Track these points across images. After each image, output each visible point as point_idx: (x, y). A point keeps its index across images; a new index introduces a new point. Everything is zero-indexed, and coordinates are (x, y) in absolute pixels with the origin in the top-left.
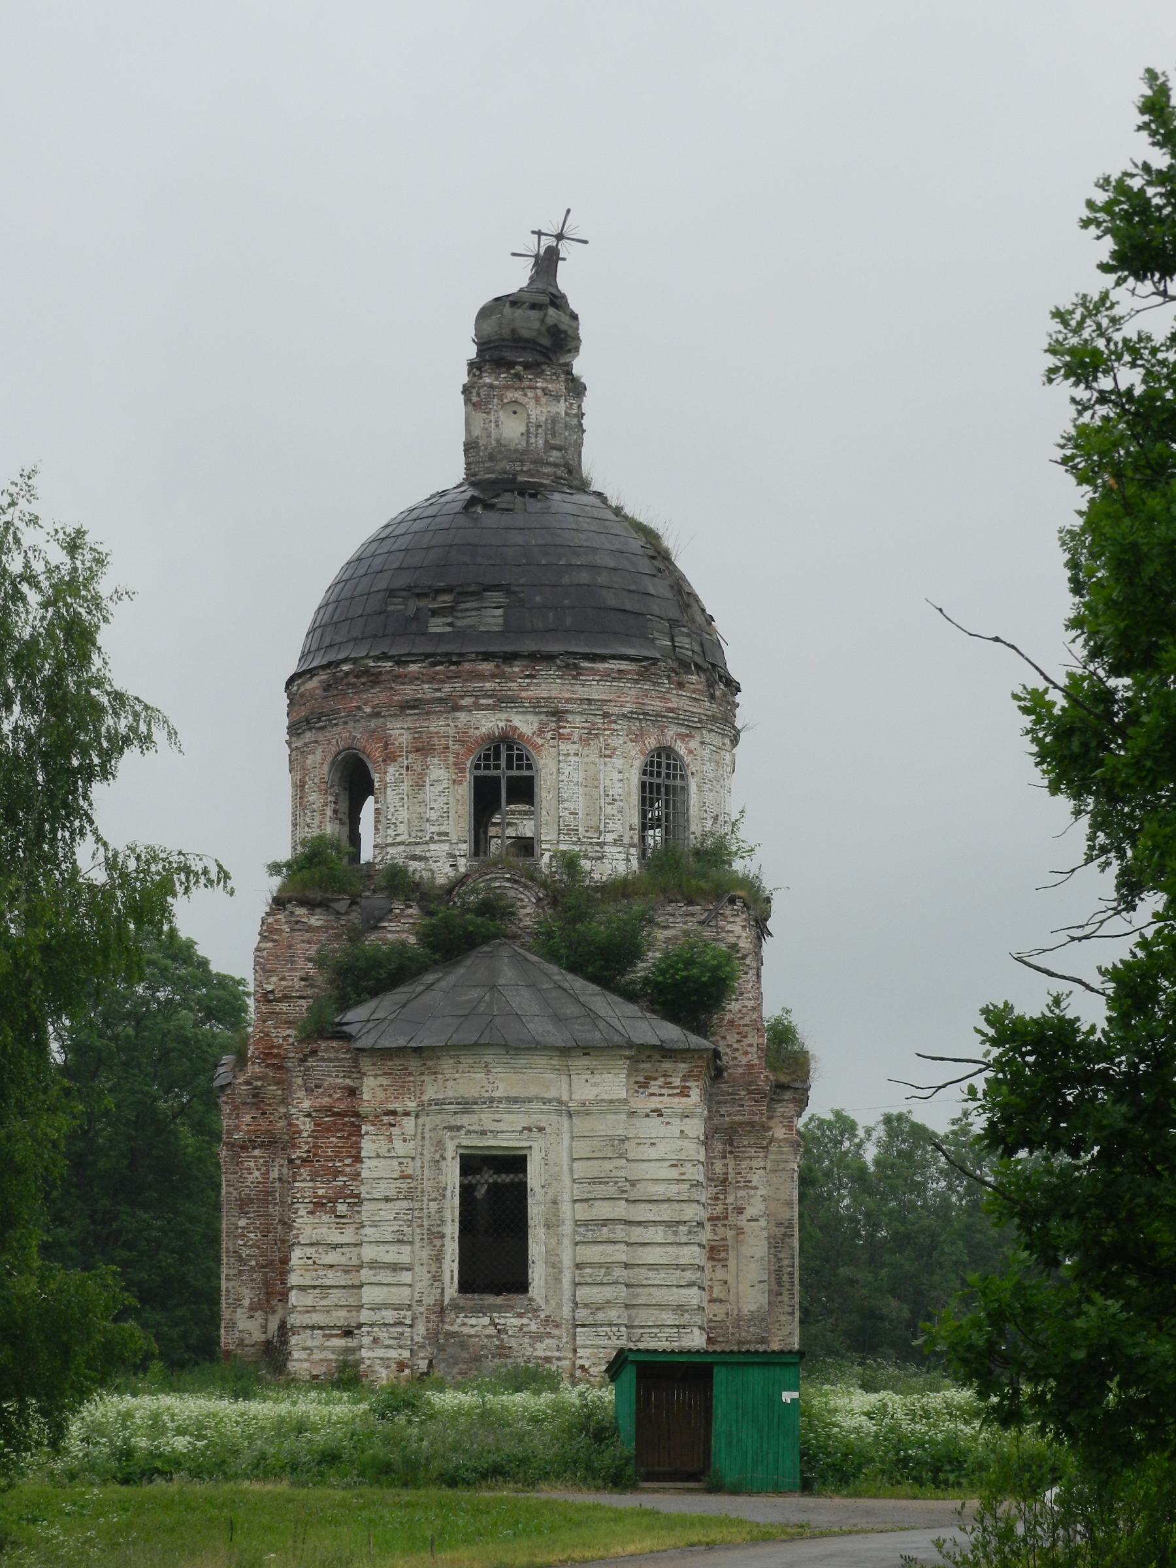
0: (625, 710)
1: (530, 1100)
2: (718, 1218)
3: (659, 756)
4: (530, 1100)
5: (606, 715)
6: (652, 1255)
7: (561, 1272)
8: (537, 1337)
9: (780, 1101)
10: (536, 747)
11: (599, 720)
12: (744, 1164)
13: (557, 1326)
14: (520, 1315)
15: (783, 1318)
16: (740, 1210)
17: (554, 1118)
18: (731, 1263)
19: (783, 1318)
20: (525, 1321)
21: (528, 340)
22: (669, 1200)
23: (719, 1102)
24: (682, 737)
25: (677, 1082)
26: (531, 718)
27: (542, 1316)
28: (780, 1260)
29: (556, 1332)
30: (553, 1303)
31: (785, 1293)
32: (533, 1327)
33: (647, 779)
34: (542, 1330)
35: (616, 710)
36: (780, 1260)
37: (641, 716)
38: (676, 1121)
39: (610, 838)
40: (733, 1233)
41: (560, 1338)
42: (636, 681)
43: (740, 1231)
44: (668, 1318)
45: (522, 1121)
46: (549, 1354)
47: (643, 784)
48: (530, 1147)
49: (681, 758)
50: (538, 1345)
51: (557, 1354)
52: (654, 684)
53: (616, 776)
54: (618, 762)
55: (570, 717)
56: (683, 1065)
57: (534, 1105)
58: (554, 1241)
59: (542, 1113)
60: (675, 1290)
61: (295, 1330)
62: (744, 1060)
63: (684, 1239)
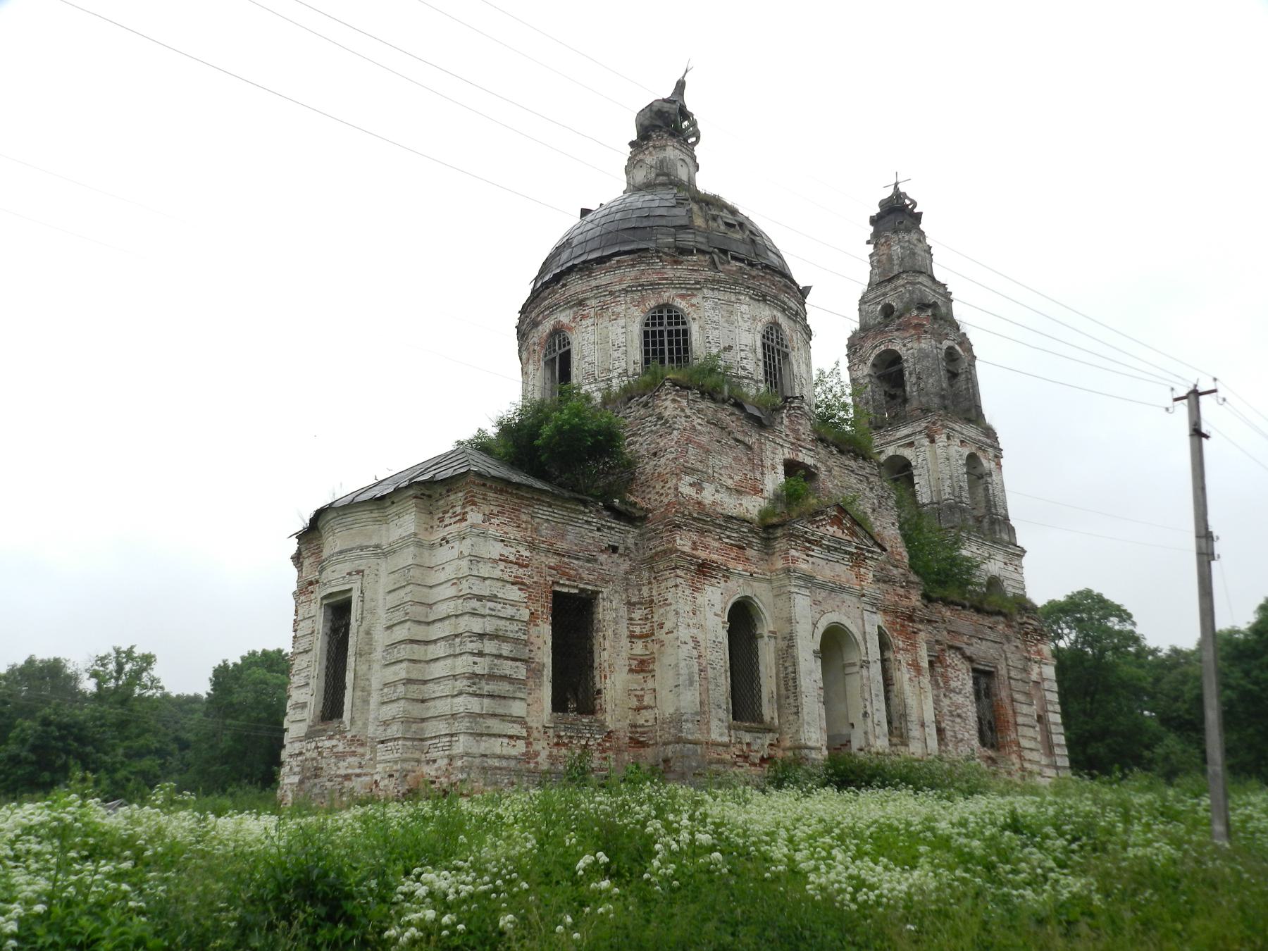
0: (624, 286)
1: (351, 550)
2: (647, 636)
3: (660, 312)
4: (351, 550)
5: (611, 293)
6: (438, 670)
7: (369, 695)
8: (341, 757)
9: (776, 538)
10: (570, 329)
11: (608, 298)
12: (663, 585)
13: (362, 745)
14: (331, 738)
15: (791, 718)
16: (661, 626)
17: (373, 561)
18: (657, 673)
19: (791, 718)
20: (334, 742)
21: (666, 124)
22: (449, 617)
23: (649, 539)
24: (683, 297)
25: (458, 510)
26: (568, 312)
27: (349, 737)
28: (786, 668)
29: (360, 750)
30: (360, 723)
31: (792, 696)
32: (341, 748)
33: (650, 329)
34: (347, 749)
35: (617, 288)
36: (786, 668)
37: (638, 287)
38: (456, 544)
39: (615, 374)
40: (657, 646)
41: (363, 755)
42: (633, 266)
43: (662, 643)
44: (443, 728)
45: (348, 567)
46: (350, 771)
47: (646, 334)
48: (350, 590)
49: (682, 310)
50: (341, 764)
51: (358, 771)
52: (648, 264)
53: (620, 330)
54: (621, 322)
55: (588, 302)
56: (460, 494)
57: (354, 553)
58: (365, 667)
59: (361, 558)
60: (449, 700)
61: (838, 744)
62: (666, 501)
63: (458, 652)
